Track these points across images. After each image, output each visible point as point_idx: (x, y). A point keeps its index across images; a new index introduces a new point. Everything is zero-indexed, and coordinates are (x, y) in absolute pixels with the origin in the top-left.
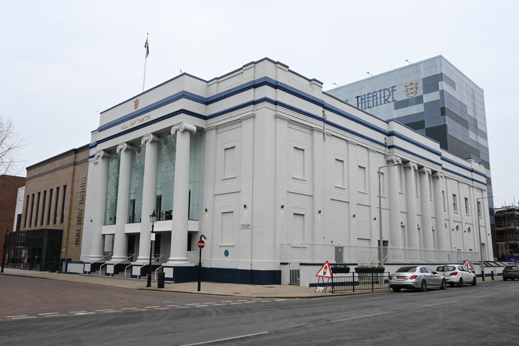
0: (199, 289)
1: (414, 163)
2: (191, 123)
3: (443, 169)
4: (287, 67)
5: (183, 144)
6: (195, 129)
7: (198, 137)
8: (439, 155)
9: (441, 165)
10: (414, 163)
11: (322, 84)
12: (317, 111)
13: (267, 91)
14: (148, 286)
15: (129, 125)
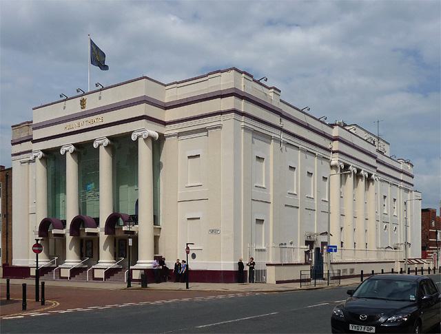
0: (187, 287)
1: (354, 167)
2: (153, 131)
3: (378, 171)
4: (251, 76)
5: (145, 152)
6: (157, 135)
7: (157, 144)
8: (374, 157)
9: (376, 168)
10: (354, 167)
11: (280, 91)
12: (275, 119)
13: (230, 103)
14: (128, 287)
15: (75, 125)
